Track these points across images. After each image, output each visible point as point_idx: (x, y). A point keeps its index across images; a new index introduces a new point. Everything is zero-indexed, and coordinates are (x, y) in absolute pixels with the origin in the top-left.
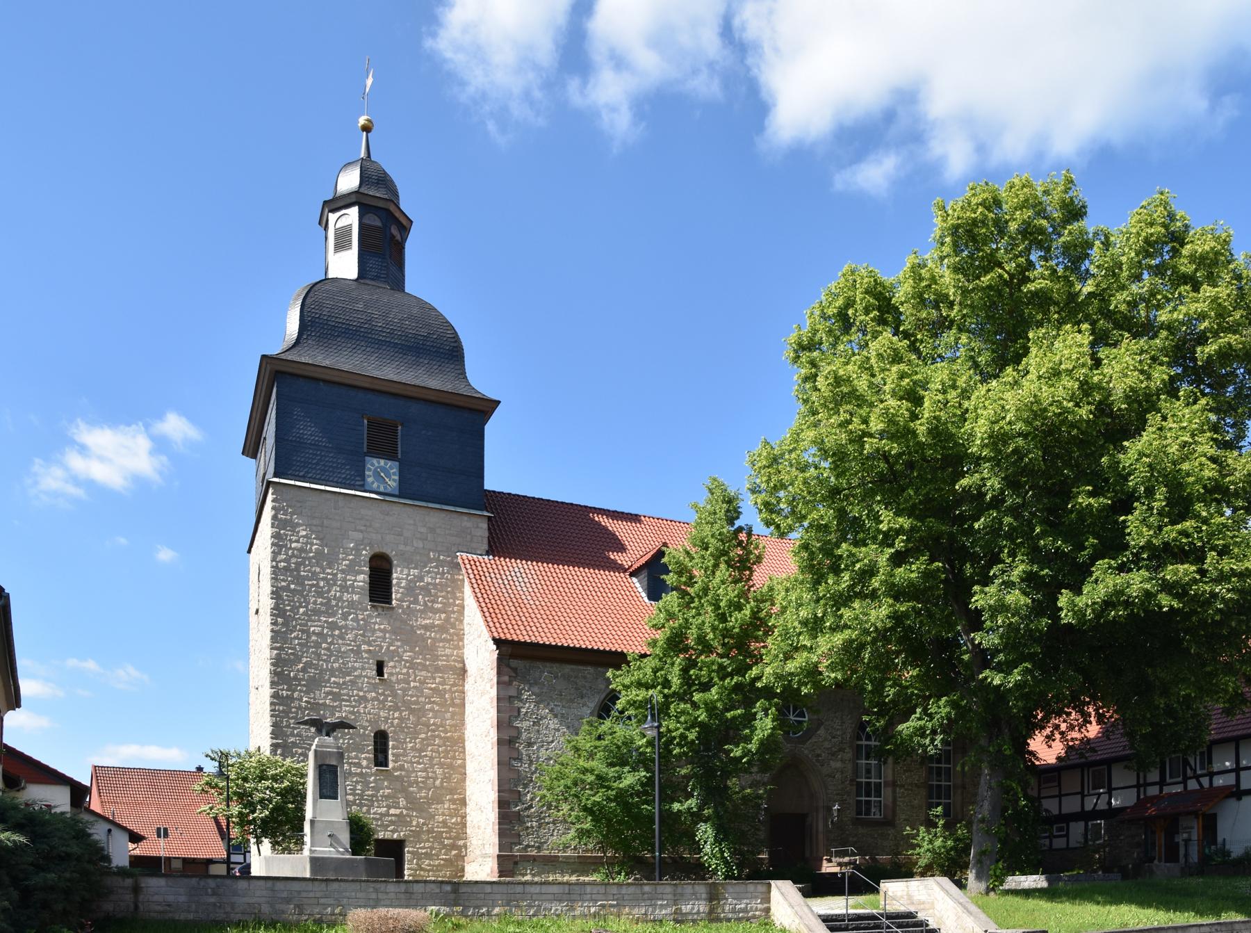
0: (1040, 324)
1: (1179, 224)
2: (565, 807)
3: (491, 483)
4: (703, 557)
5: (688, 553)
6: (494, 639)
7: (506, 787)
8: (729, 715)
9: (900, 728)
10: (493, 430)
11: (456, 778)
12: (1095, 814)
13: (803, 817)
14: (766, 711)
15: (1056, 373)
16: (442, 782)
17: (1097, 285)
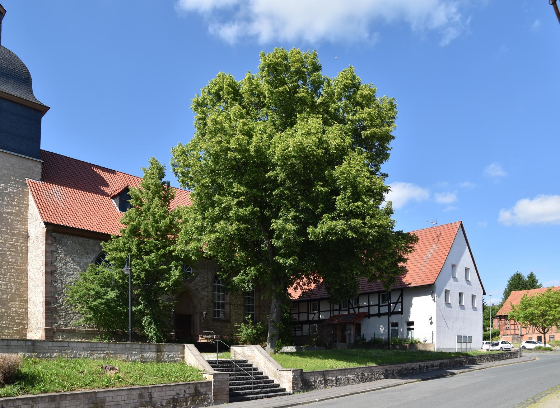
0: (300, 112)
1: (357, 81)
2: (79, 306)
3: (43, 147)
4: (147, 193)
5: (140, 191)
6: (44, 222)
7: (50, 295)
8: (160, 268)
9: (234, 279)
10: (45, 120)
11: (23, 289)
12: (313, 322)
13: (190, 316)
14: (176, 267)
15: (309, 134)
16: (15, 291)
17: (324, 100)
